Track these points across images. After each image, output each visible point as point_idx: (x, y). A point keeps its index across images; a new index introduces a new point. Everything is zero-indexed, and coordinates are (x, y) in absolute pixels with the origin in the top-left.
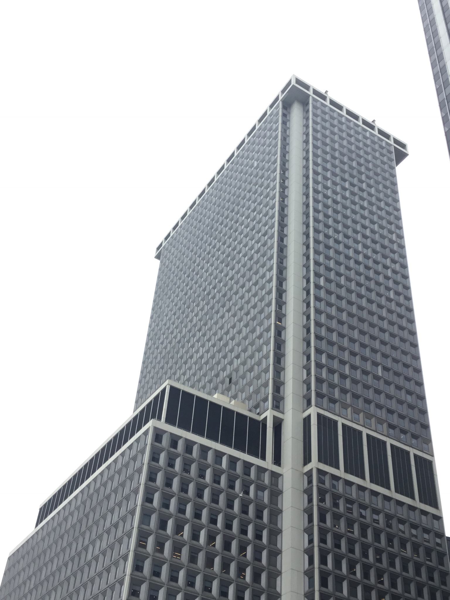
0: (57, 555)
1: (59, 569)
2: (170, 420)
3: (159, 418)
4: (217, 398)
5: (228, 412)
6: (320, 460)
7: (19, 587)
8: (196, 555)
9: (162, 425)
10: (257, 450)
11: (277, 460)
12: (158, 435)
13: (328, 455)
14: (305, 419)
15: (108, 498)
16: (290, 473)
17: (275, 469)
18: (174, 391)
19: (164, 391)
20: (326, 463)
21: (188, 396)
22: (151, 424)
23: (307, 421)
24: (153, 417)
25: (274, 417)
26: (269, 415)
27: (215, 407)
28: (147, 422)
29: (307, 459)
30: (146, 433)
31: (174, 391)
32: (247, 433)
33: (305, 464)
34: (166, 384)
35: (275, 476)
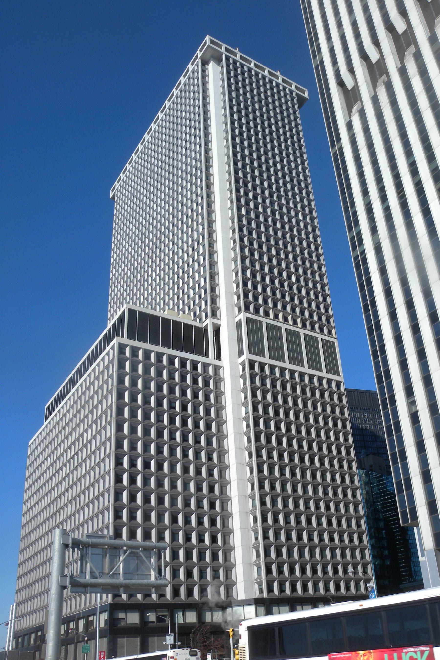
0: (63, 441)
1: (66, 451)
2: (131, 336)
3: (123, 336)
4: (166, 314)
5: (177, 324)
6: (250, 353)
7: (40, 465)
8: (278, 653)
9: (125, 340)
10: (202, 350)
11: (219, 356)
12: (122, 348)
13: (255, 347)
14: (237, 323)
15: (92, 398)
16: (231, 364)
17: (217, 363)
18: (132, 312)
19: (123, 313)
20: (255, 354)
21: (143, 315)
22: (115, 342)
23: (239, 324)
24: (118, 335)
25: (247, 318)
26: (209, 322)
27: (166, 321)
28: (113, 338)
29: (241, 353)
30: (113, 348)
31: (132, 312)
32: (191, 339)
33: (240, 357)
34: (124, 308)
35: (217, 369)
